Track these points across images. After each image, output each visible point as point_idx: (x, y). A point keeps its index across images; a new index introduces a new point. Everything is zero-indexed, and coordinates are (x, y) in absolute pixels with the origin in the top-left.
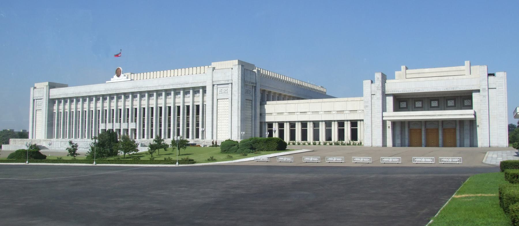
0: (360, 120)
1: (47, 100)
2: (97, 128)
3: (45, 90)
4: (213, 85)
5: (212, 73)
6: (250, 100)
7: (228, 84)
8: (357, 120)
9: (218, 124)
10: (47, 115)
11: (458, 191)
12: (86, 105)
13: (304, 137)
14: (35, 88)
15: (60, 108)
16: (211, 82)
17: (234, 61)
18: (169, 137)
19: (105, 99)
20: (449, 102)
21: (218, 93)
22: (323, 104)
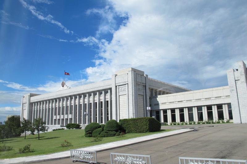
4: (116, 86)
7: (125, 85)
8: (222, 104)
13: (182, 119)
18: (85, 122)
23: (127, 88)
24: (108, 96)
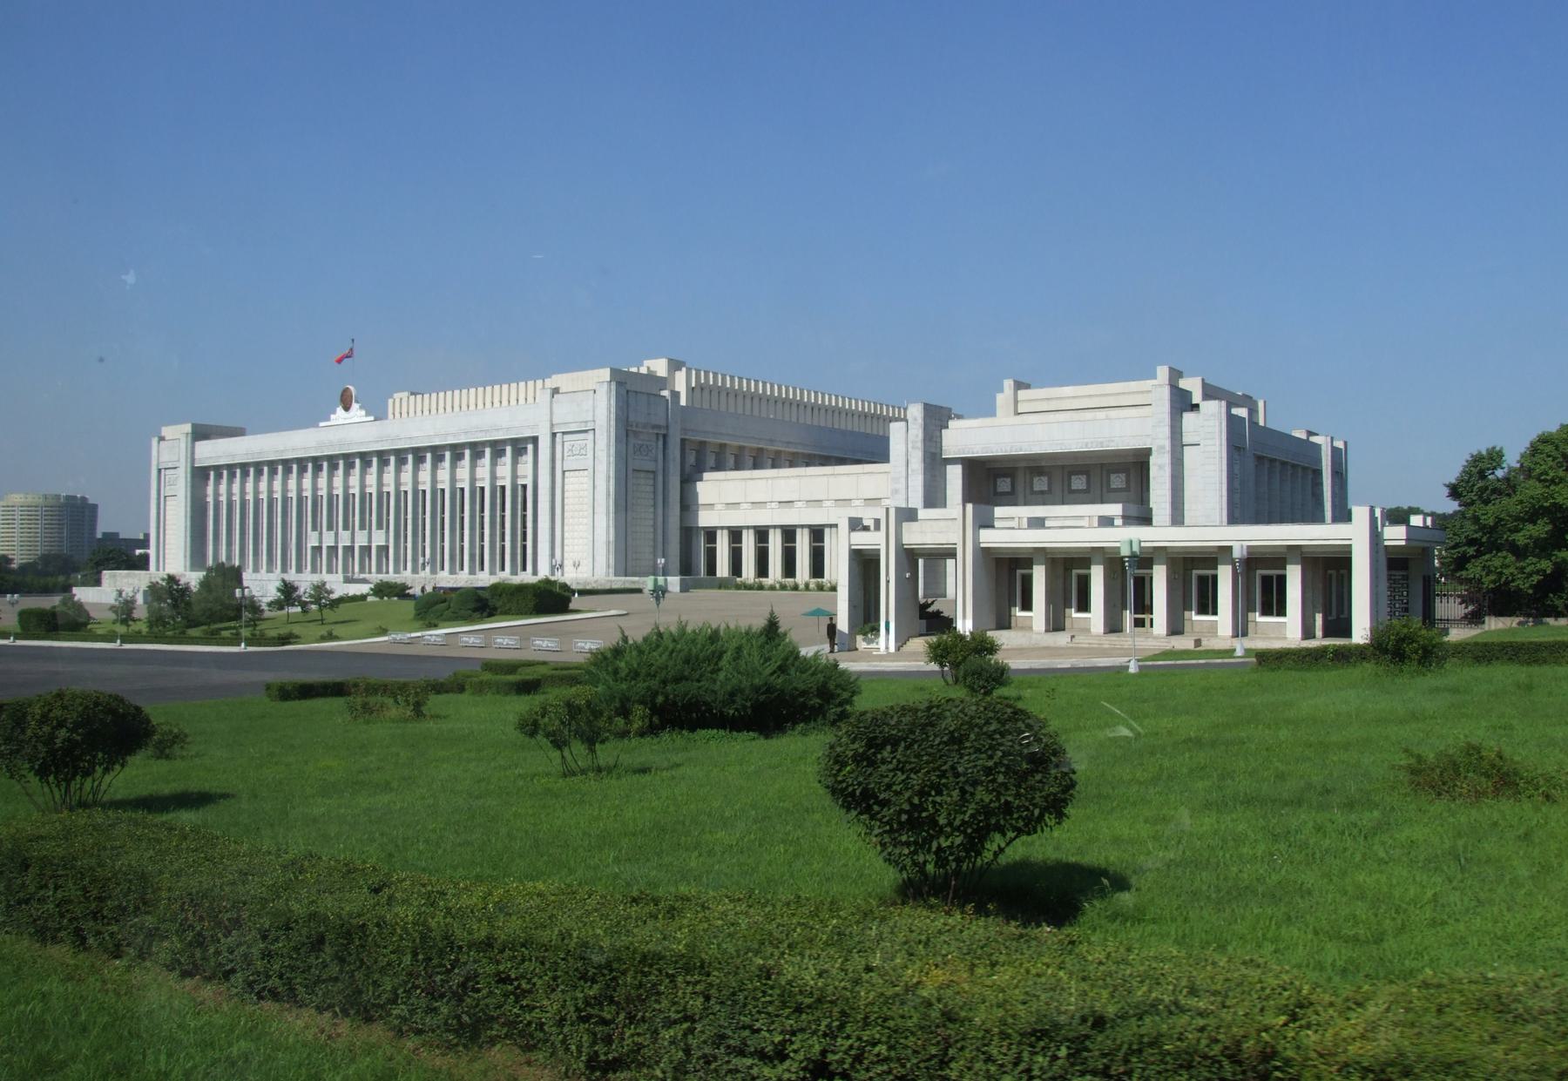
0: (831, 526)
1: (189, 470)
2: (498, 539)
3: (183, 445)
4: (554, 435)
5: (551, 402)
6: (648, 471)
7: (586, 431)
9: (566, 535)
10: (189, 509)
11: (395, 639)
12: (463, 472)
14: (162, 439)
15: (351, 484)
16: (548, 425)
17: (602, 371)
19: (441, 458)
20: (1113, 477)
21: (566, 454)
22: (832, 479)
23: (590, 445)
24: (526, 466)
